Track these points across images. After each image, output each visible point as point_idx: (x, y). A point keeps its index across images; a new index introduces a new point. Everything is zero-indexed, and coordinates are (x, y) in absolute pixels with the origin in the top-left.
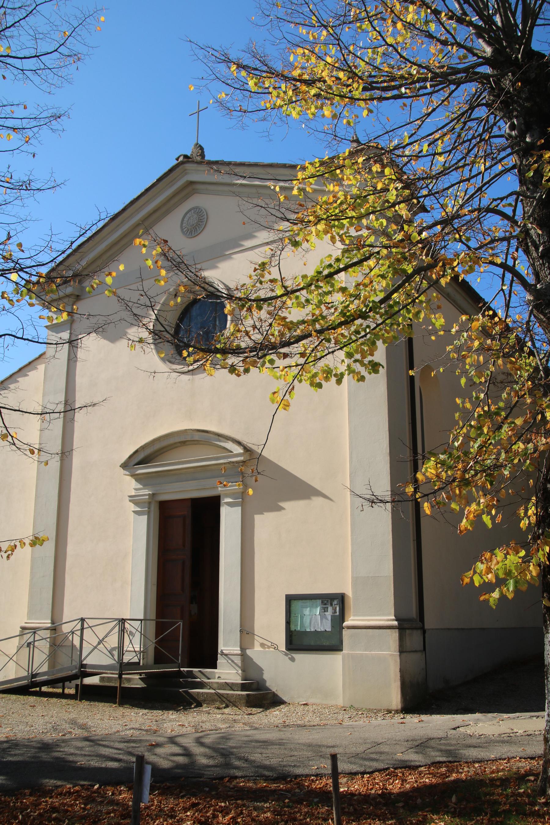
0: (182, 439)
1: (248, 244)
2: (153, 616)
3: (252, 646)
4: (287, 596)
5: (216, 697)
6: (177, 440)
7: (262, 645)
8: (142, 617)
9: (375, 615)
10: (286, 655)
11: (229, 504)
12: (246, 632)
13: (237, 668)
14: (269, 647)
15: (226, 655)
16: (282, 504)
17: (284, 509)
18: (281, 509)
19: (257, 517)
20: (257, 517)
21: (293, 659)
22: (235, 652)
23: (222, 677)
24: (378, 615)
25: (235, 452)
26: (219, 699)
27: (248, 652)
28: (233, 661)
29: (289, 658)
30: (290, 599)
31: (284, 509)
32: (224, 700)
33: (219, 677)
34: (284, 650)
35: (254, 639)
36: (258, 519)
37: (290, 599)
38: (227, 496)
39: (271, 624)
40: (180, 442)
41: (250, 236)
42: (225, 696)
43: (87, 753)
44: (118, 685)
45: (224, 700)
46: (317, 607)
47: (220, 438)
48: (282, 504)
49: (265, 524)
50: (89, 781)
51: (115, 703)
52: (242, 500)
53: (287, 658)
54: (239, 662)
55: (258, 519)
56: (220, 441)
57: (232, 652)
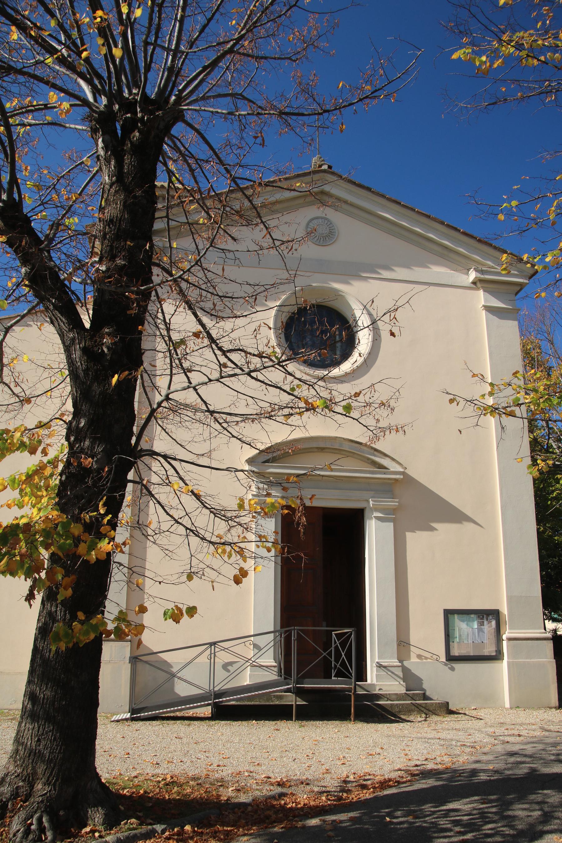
0: (322, 445)
1: (386, 274)
2: (279, 628)
3: (409, 657)
4: (445, 610)
5: (413, 707)
6: (314, 445)
7: (419, 656)
8: (272, 630)
9: (528, 629)
10: (446, 665)
11: (377, 518)
12: (403, 644)
13: (399, 680)
14: (426, 658)
15: (385, 667)
16: (434, 525)
17: (436, 530)
18: (433, 529)
19: (409, 535)
20: (409, 535)
21: (453, 669)
22: (395, 664)
23: (384, 688)
24: (525, 629)
25: (392, 470)
26: (416, 709)
27: (406, 663)
28: (393, 673)
29: (449, 668)
30: (448, 614)
31: (436, 530)
32: (423, 709)
33: (380, 689)
34: (444, 660)
35: (409, 651)
36: (409, 536)
37: (448, 614)
38: (377, 510)
39: (427, 636)
40: (317, 448)
41: (387, 268)
42: (423, 706)
43: (524, 765)
44: (294, 703)
45: (423, 709)
46: (474, 621)
47: (376, 453)
48: (434, 525)
49: (415, 541)
50: (478, 796)
51: (350, 720)
52: (390, 515)
53: (446, 668)
54: (401, 674)
55: (409, 536)
56: (375, 456)
57: (391, 664)
